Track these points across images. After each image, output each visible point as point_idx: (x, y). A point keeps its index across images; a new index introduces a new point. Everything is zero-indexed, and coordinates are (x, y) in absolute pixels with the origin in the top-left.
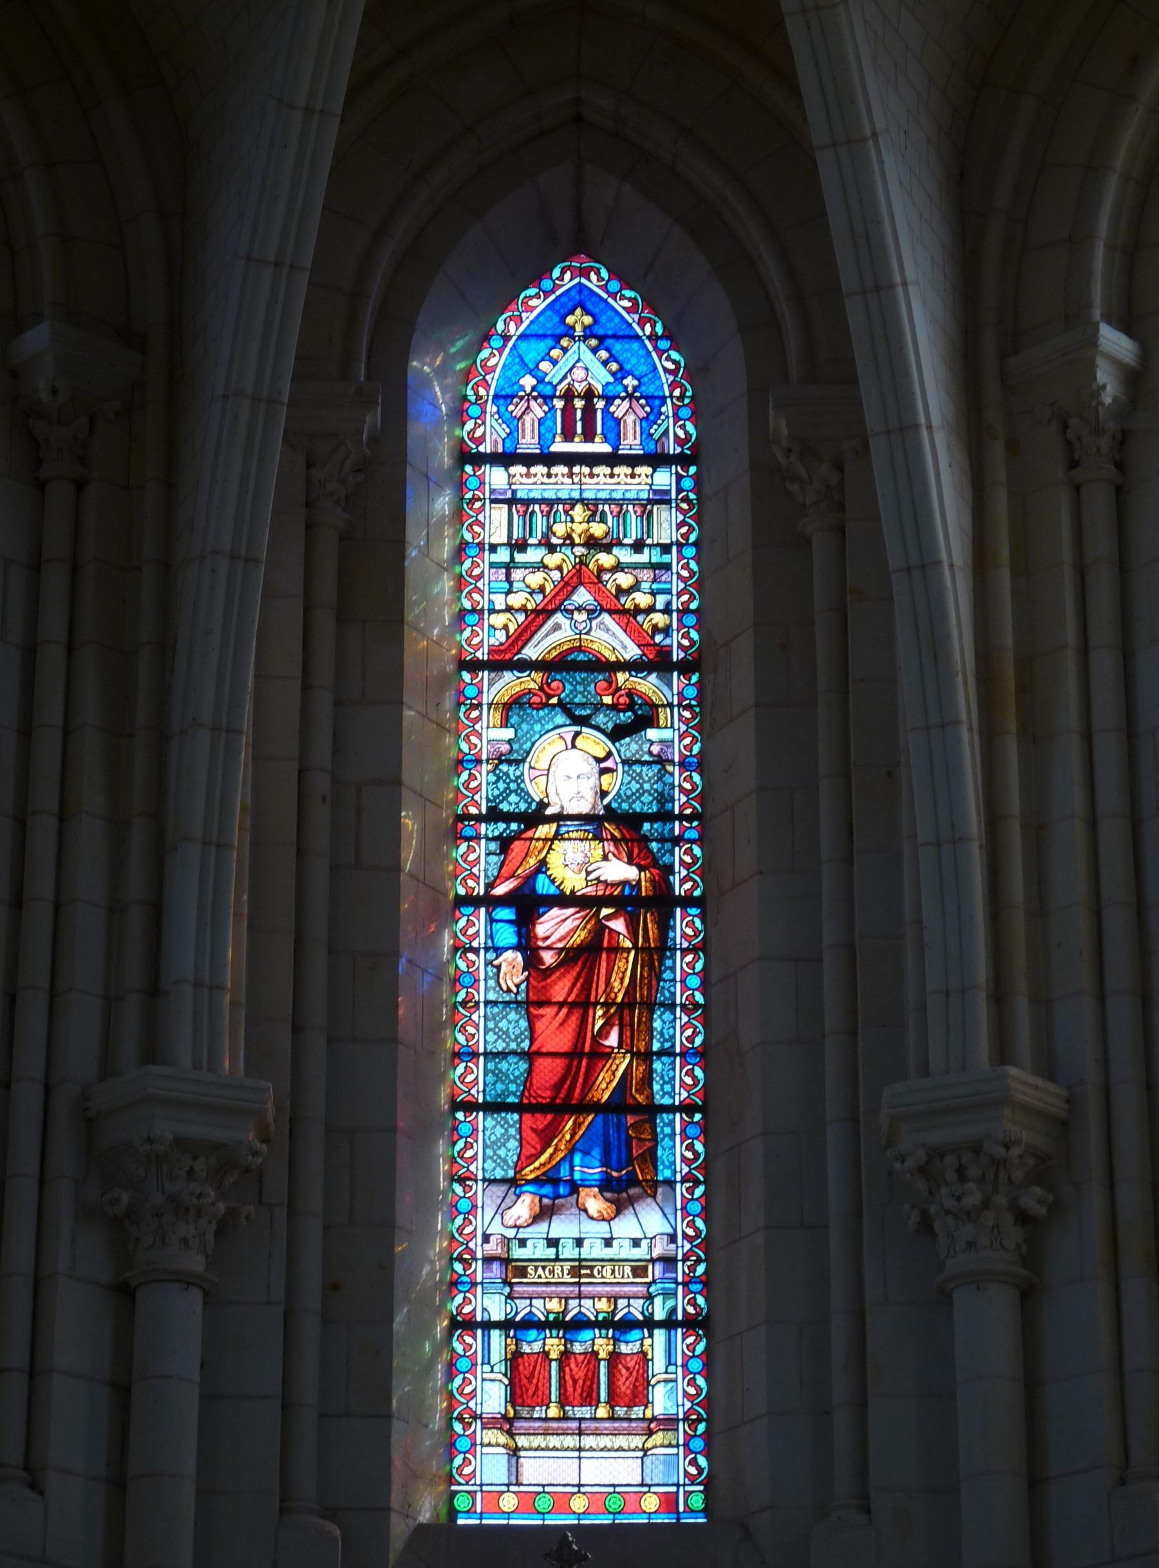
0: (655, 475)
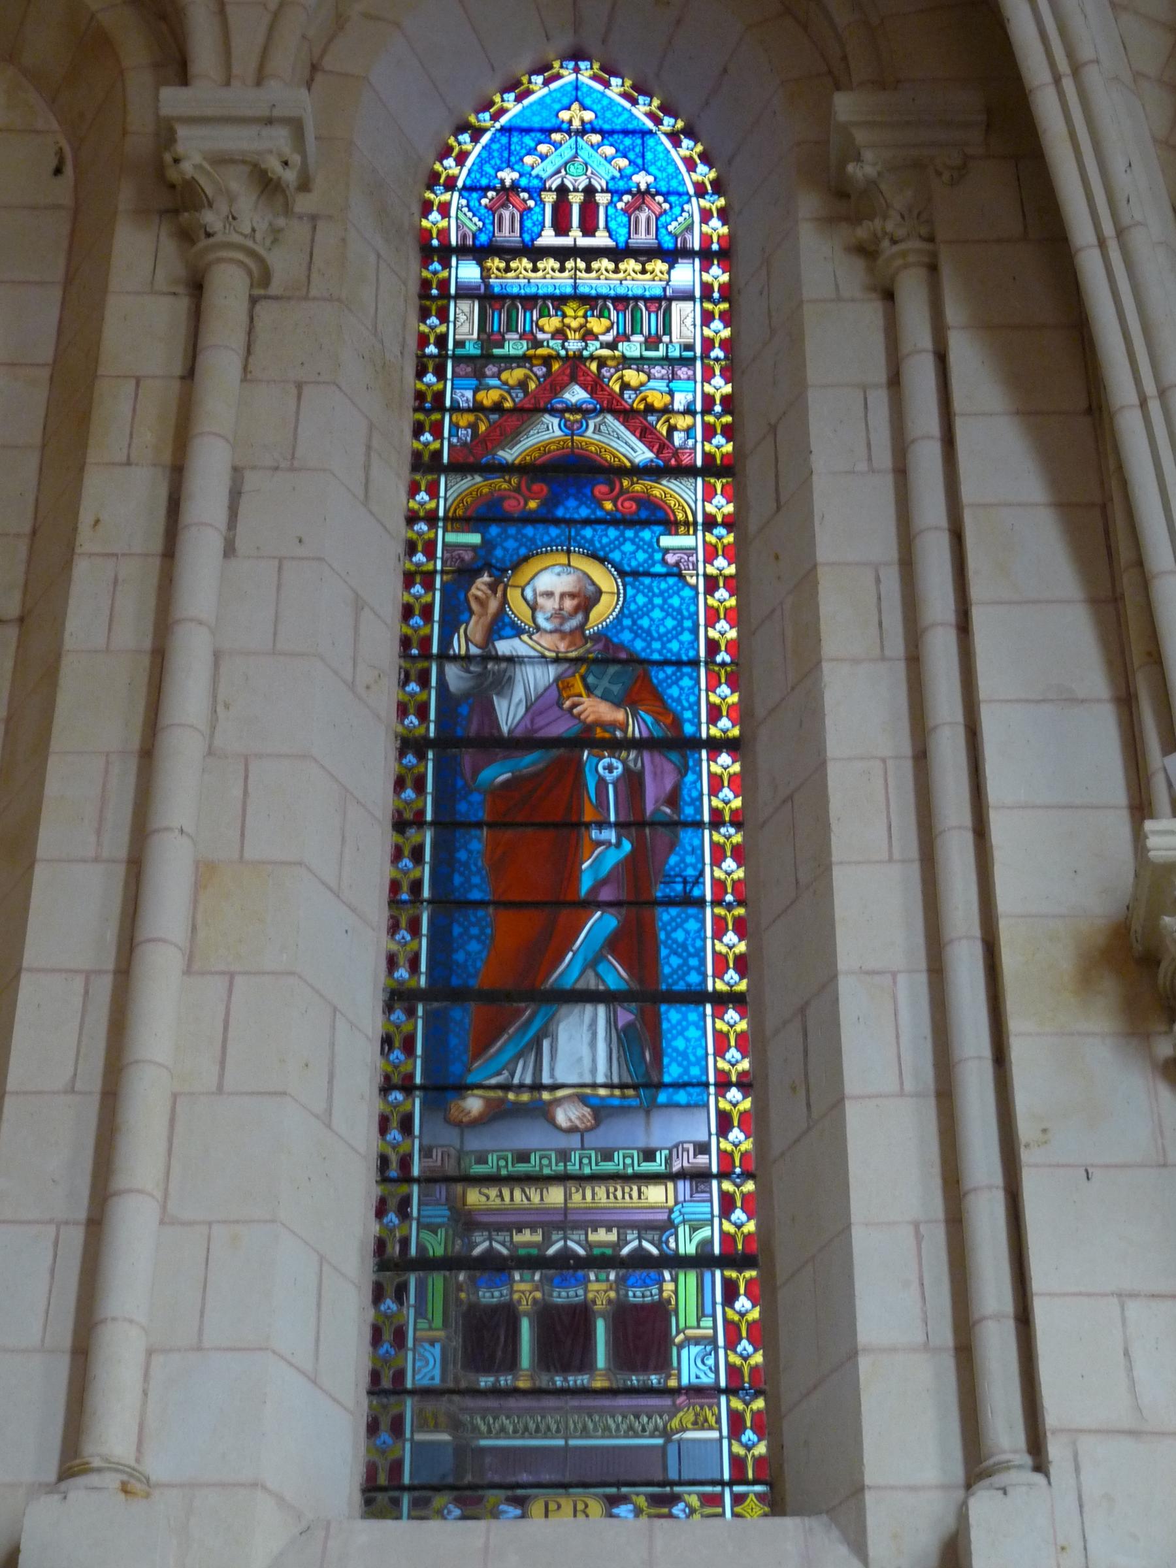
0: (672, 272)
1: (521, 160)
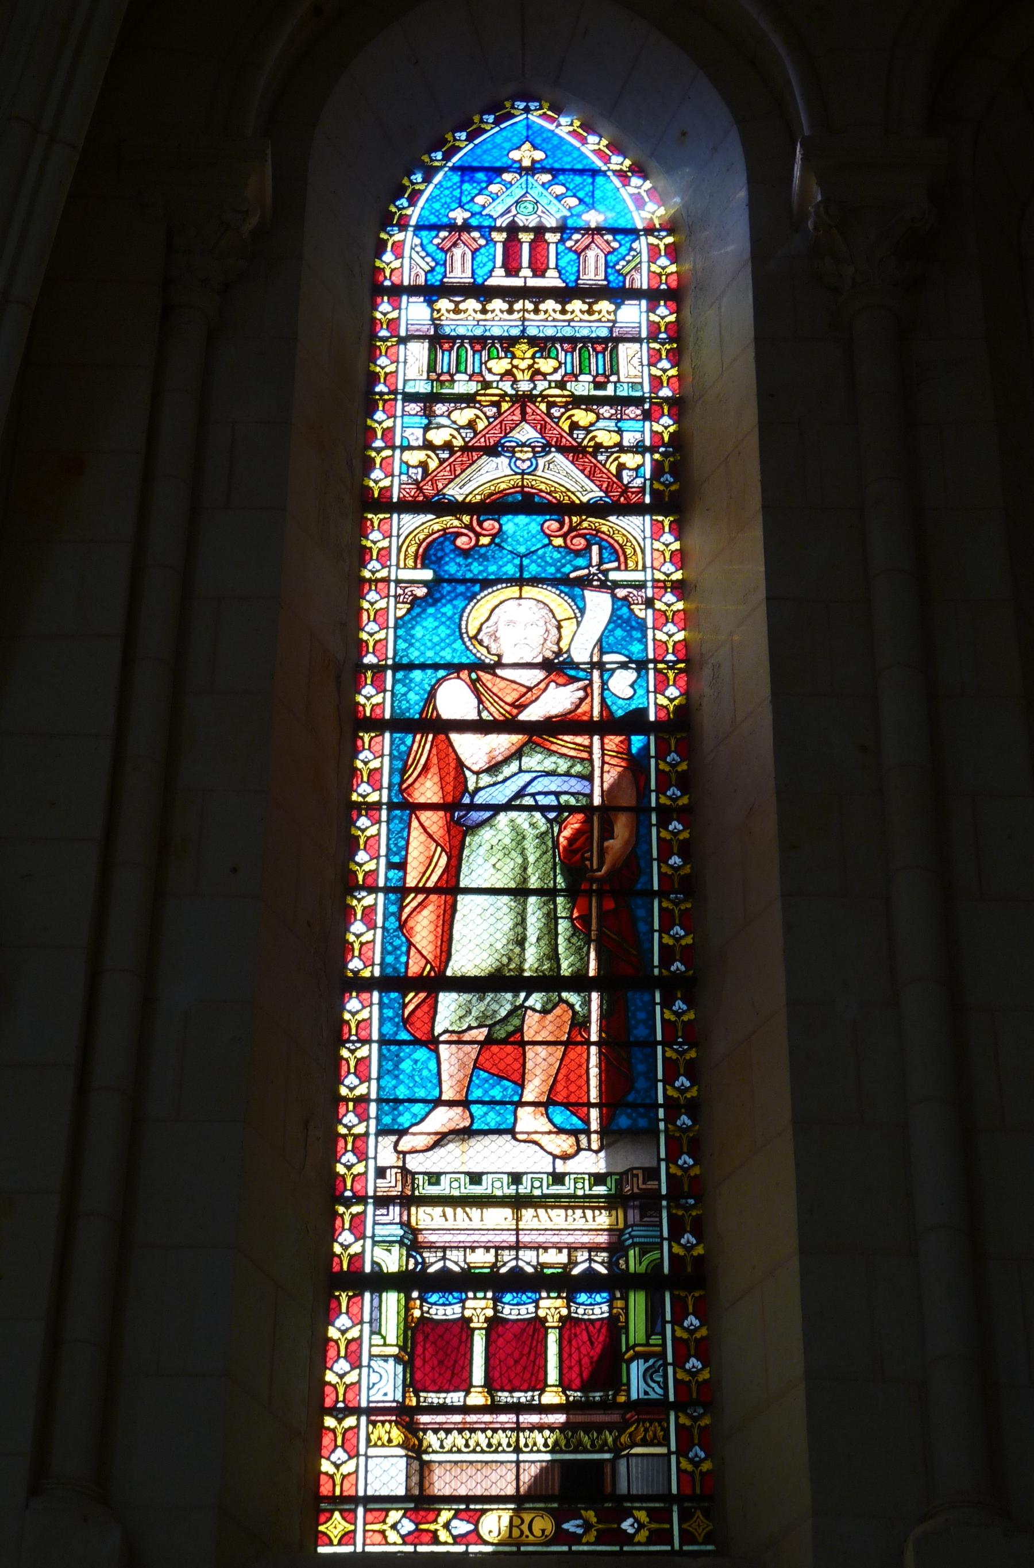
0: (619, 312)
1: (472, 200)
